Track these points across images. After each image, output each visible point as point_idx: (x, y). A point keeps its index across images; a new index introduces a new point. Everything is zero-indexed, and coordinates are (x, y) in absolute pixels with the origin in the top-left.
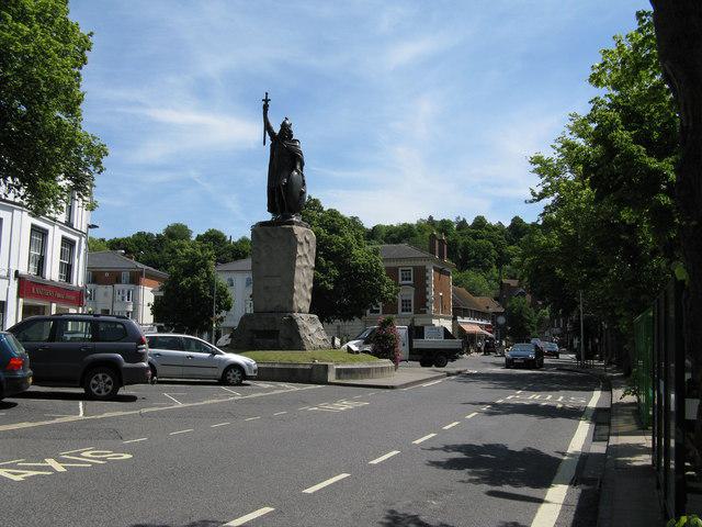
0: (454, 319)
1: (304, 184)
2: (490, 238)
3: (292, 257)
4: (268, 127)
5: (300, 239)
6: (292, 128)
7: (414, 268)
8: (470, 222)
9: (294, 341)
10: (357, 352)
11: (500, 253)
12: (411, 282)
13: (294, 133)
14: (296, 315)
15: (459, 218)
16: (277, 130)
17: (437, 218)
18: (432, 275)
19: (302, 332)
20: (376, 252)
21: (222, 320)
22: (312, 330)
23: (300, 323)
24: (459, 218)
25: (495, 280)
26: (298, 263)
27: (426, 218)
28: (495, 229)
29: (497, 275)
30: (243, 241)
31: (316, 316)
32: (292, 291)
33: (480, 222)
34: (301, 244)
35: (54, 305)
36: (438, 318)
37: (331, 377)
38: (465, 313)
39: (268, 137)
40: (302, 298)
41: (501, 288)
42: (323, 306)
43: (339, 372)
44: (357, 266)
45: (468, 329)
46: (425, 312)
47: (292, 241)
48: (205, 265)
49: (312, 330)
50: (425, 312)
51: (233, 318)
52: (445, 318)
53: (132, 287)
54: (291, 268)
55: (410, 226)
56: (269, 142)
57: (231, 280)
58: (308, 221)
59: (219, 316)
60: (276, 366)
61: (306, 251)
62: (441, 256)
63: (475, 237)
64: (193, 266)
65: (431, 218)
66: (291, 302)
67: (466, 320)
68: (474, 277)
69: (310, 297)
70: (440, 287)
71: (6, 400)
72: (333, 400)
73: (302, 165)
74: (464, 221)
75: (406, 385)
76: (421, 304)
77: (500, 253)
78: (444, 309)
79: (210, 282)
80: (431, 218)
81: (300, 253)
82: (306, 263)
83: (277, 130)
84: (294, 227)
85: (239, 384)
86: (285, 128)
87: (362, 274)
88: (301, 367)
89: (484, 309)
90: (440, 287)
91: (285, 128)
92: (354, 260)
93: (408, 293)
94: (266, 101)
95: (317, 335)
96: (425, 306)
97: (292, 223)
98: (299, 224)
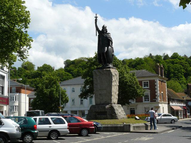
0: (169, 104)
1: (113, 52)
2: (181, 63)
3: (110, 82)
4: (97, 29)
5: (113, 74)
6: (107, 28)
7: (150, 81)
8: (170, 56)
9: (112, 115)
10: (139, 119)
11: (186, 70)
12: (148, 87)
13: (108, 30)
14: (113, 105)
15: (164, 54)
16: (101, 29)
17: (154, 54)
18: (158, 83)
19: (116, 112)
20: (133, 75)
21: (63, 107)
22: (120, 111)
23: (115, 108)
24: (164, 54)
25: (185, 84)
26: (113, 84)
27: (148, 55)
28: (183, 59)
29: (185, 81)
30: (61, 69)
31: (120, 105)
32: (111, 95)
33: (175, 56)
34: (114, 76)
35: (188, 114)
36: (162, 103)
37: (132, 130)
38: (173, 100)
39: (97, 32)
40: (115, 98)
41: (188, 88)
42: (122, 101)
43: (134, 127)
44: (127, 82)
45: (175, 108)
46: (155, 101)
47: (110, 75)
48: (55, 83)
49: (120, 111)
50: (155, 101)
51: (155, 112)
52: (165, 103)
53: (18, 94)
54: (110, 86)
55: (141, 59)
56: (98, 34)
57: (73, 89)
58: (116, 66)
59: (62, 106)
60: (109, 126)
61: (115, 79)
62: (162, 75)
63: (173, 63)
64: (51, 83)
65: (151, 55)
66: (111, 100)
67: (174, 104)
68: (175, 83)
69: (117, 98)
70: (162, 88)
71: (97, 132)
72: (140, 137)
73: (112, 43)
74: (167, 55)
75: (162, 132)
76: (153, 98)
77: (186, 70)
78: (164, 99)
79: (57, 90)
80: (151, 55)
81: (113, 80)
82: (115, 84)
83: (101, 29)
84: (111, 69)
85: (87, 136)
86: (104, 28)
87: (129, 85)
88: (119, 126)
89: (181, 99)
90: (162, 88)
91: (104, 28)
92: (126, 79)
93: (148, 92)
94: (96, 17)
95: (122, 113)
96: (155, 98)
97: (110, 68)
98: (112, 68)
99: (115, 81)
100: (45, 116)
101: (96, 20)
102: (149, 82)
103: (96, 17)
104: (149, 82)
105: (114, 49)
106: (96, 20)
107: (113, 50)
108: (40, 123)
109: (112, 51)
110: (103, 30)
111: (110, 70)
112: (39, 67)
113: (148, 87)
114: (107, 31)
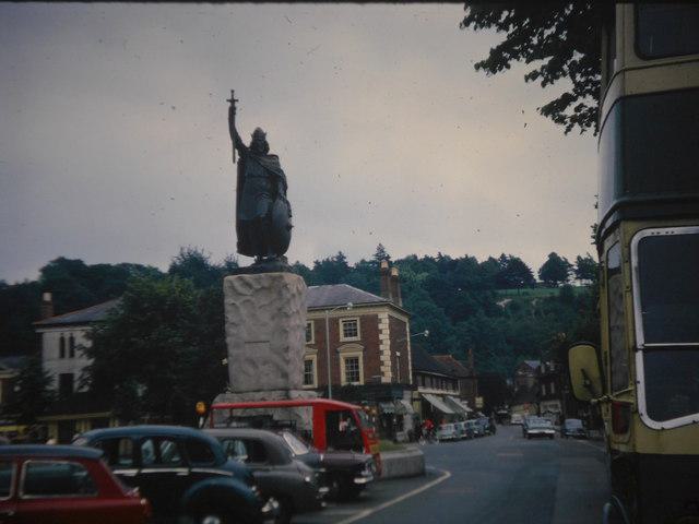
12: (358, 338)
16: (247, 141)
39: (236, 151)
40: (408, 325)
56: (238, 157)
73: (285, 188)
82: (298, 322)
83: (247, 141)
86: (259, 136)
91: (259, 136)
94: (233, 101)
99: (298, 312)
100: (142, 422)
101: (232, 111)
102: (358, 323)
103: (233, 101)
104: (358, 323)
105: (292, 208)
106: (232, 111)
107: (290, 211)
108: (397, 328)
109: (286, 213)
110: (253, 143)
111: (281, 277)
112: (321, 260)
113: (358, 338)
114: (267, 149)
